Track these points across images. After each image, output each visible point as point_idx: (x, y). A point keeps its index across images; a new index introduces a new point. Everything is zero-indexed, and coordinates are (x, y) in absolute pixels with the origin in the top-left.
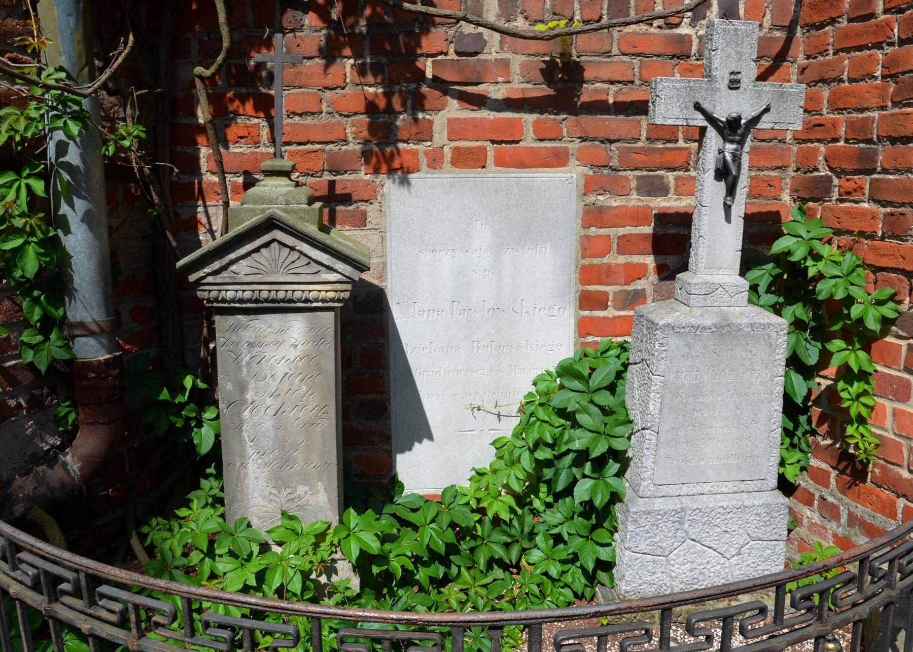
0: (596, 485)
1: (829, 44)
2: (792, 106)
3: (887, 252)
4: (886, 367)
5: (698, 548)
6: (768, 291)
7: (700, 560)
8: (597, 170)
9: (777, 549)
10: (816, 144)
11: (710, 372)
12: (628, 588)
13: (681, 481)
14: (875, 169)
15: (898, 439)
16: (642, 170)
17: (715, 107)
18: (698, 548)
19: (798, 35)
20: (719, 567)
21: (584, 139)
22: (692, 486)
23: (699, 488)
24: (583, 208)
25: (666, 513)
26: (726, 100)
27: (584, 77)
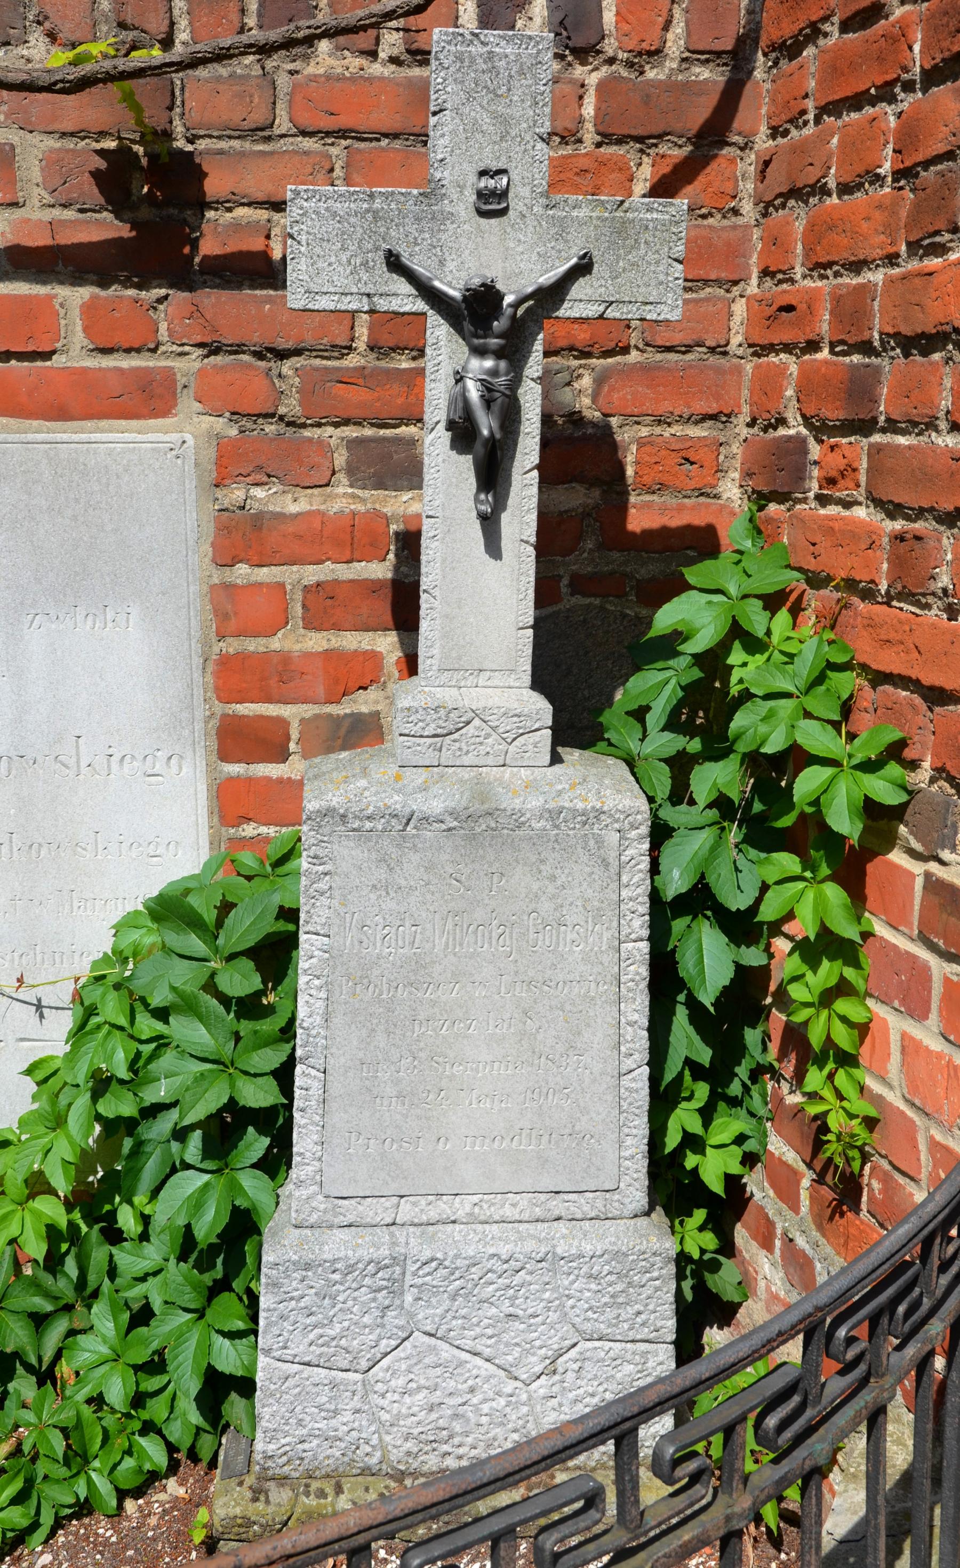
1: (806, 96)
2: (651, 257)
3: (892, 636)
4: (891, 926)
5: (444, 1355)
6: (672, 724)
7: (452, 1383)
8: (249, 425)
9: (650, 1364)
10: (782, 356)
11: (449, 926)
12: (272, 1447)
13: (393, 1188)
14: (874, 420)
15: (910, 1113)
16: (359, 424)
17: (442, 263)
18: (444, 1355)
19: (758, 74)
20: (502, 1401)
21: (213, 349)
22: (423, 1201)
23: (443, 1208)
25: (351, 1269)
26: (471, 245)
27: (204, 194)
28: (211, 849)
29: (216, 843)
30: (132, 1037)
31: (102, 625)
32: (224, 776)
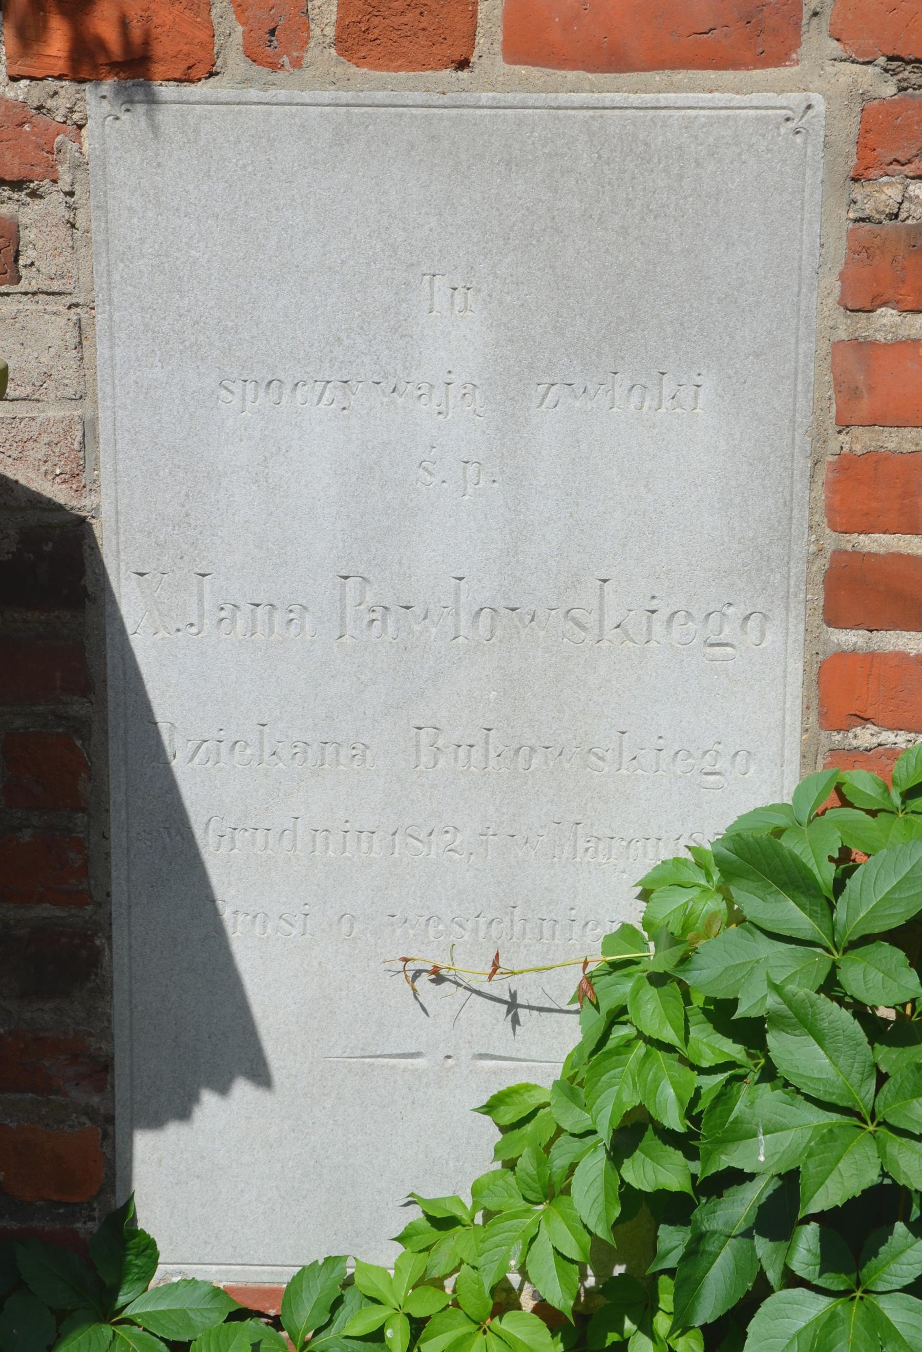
0: (831, 1321)
24: (851, 233)
28: (803, 765)
29: (811, 756)
30: (684, 1061)
31: (655, 404)
32: (830, 650)
